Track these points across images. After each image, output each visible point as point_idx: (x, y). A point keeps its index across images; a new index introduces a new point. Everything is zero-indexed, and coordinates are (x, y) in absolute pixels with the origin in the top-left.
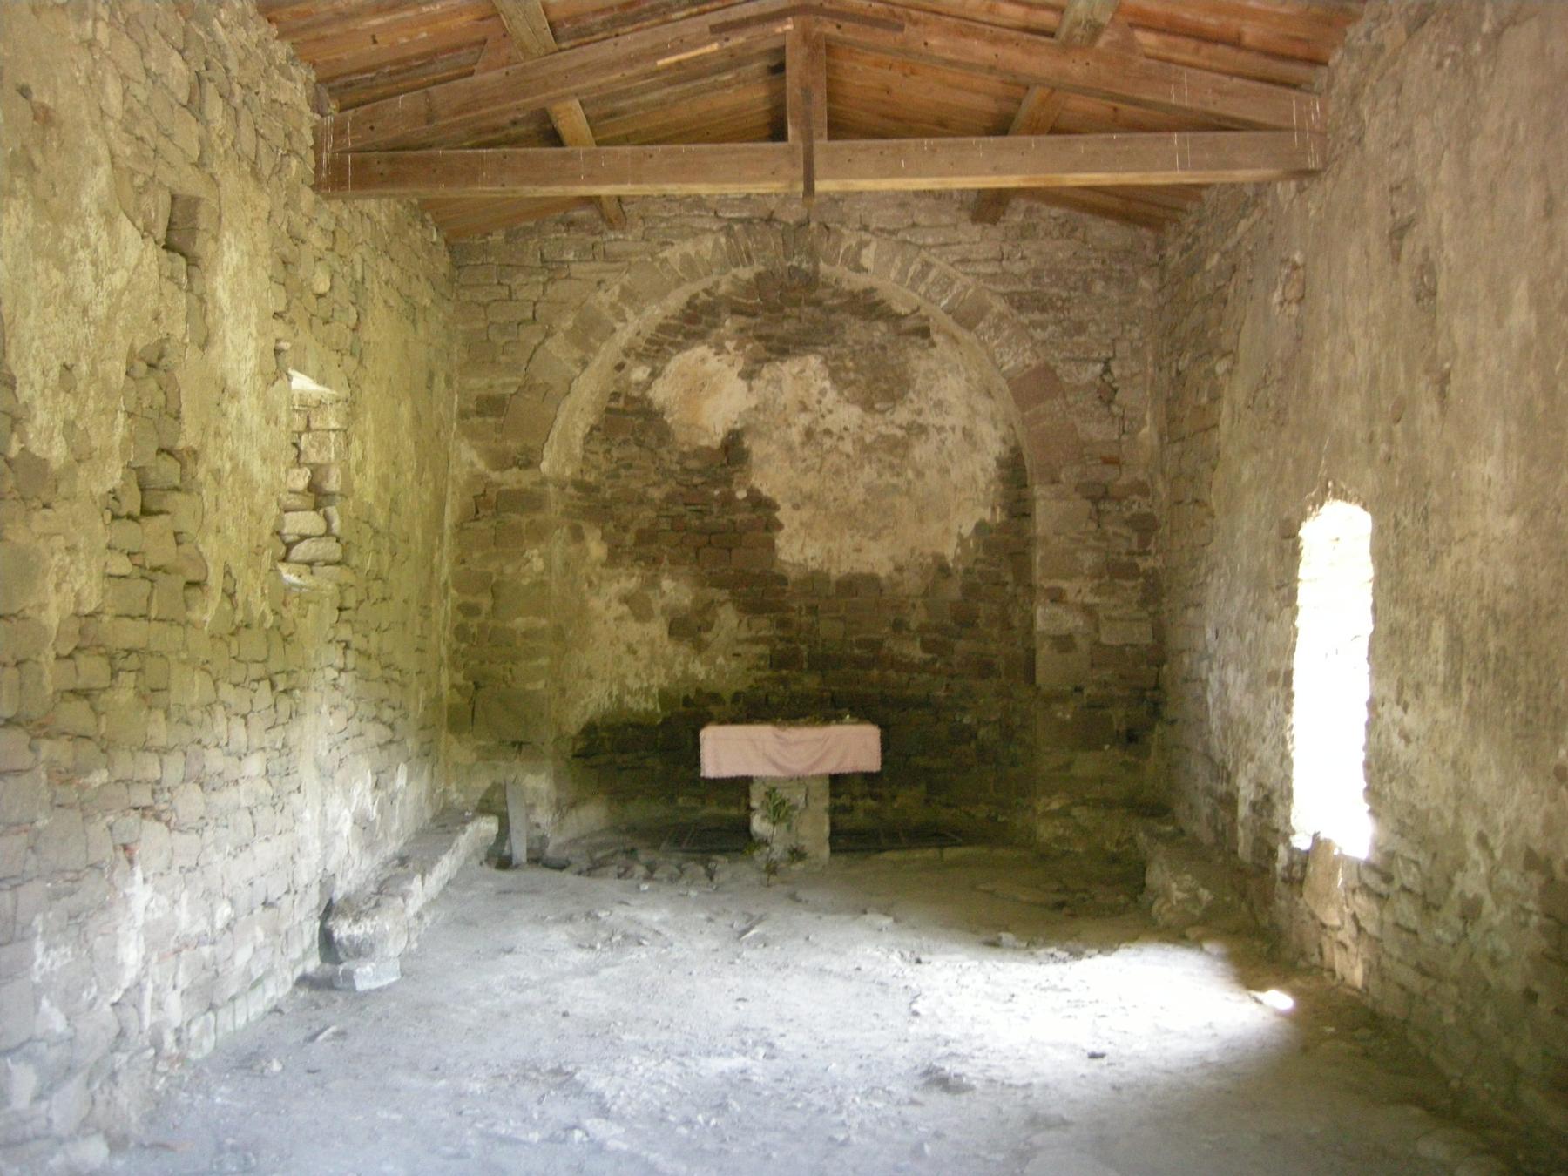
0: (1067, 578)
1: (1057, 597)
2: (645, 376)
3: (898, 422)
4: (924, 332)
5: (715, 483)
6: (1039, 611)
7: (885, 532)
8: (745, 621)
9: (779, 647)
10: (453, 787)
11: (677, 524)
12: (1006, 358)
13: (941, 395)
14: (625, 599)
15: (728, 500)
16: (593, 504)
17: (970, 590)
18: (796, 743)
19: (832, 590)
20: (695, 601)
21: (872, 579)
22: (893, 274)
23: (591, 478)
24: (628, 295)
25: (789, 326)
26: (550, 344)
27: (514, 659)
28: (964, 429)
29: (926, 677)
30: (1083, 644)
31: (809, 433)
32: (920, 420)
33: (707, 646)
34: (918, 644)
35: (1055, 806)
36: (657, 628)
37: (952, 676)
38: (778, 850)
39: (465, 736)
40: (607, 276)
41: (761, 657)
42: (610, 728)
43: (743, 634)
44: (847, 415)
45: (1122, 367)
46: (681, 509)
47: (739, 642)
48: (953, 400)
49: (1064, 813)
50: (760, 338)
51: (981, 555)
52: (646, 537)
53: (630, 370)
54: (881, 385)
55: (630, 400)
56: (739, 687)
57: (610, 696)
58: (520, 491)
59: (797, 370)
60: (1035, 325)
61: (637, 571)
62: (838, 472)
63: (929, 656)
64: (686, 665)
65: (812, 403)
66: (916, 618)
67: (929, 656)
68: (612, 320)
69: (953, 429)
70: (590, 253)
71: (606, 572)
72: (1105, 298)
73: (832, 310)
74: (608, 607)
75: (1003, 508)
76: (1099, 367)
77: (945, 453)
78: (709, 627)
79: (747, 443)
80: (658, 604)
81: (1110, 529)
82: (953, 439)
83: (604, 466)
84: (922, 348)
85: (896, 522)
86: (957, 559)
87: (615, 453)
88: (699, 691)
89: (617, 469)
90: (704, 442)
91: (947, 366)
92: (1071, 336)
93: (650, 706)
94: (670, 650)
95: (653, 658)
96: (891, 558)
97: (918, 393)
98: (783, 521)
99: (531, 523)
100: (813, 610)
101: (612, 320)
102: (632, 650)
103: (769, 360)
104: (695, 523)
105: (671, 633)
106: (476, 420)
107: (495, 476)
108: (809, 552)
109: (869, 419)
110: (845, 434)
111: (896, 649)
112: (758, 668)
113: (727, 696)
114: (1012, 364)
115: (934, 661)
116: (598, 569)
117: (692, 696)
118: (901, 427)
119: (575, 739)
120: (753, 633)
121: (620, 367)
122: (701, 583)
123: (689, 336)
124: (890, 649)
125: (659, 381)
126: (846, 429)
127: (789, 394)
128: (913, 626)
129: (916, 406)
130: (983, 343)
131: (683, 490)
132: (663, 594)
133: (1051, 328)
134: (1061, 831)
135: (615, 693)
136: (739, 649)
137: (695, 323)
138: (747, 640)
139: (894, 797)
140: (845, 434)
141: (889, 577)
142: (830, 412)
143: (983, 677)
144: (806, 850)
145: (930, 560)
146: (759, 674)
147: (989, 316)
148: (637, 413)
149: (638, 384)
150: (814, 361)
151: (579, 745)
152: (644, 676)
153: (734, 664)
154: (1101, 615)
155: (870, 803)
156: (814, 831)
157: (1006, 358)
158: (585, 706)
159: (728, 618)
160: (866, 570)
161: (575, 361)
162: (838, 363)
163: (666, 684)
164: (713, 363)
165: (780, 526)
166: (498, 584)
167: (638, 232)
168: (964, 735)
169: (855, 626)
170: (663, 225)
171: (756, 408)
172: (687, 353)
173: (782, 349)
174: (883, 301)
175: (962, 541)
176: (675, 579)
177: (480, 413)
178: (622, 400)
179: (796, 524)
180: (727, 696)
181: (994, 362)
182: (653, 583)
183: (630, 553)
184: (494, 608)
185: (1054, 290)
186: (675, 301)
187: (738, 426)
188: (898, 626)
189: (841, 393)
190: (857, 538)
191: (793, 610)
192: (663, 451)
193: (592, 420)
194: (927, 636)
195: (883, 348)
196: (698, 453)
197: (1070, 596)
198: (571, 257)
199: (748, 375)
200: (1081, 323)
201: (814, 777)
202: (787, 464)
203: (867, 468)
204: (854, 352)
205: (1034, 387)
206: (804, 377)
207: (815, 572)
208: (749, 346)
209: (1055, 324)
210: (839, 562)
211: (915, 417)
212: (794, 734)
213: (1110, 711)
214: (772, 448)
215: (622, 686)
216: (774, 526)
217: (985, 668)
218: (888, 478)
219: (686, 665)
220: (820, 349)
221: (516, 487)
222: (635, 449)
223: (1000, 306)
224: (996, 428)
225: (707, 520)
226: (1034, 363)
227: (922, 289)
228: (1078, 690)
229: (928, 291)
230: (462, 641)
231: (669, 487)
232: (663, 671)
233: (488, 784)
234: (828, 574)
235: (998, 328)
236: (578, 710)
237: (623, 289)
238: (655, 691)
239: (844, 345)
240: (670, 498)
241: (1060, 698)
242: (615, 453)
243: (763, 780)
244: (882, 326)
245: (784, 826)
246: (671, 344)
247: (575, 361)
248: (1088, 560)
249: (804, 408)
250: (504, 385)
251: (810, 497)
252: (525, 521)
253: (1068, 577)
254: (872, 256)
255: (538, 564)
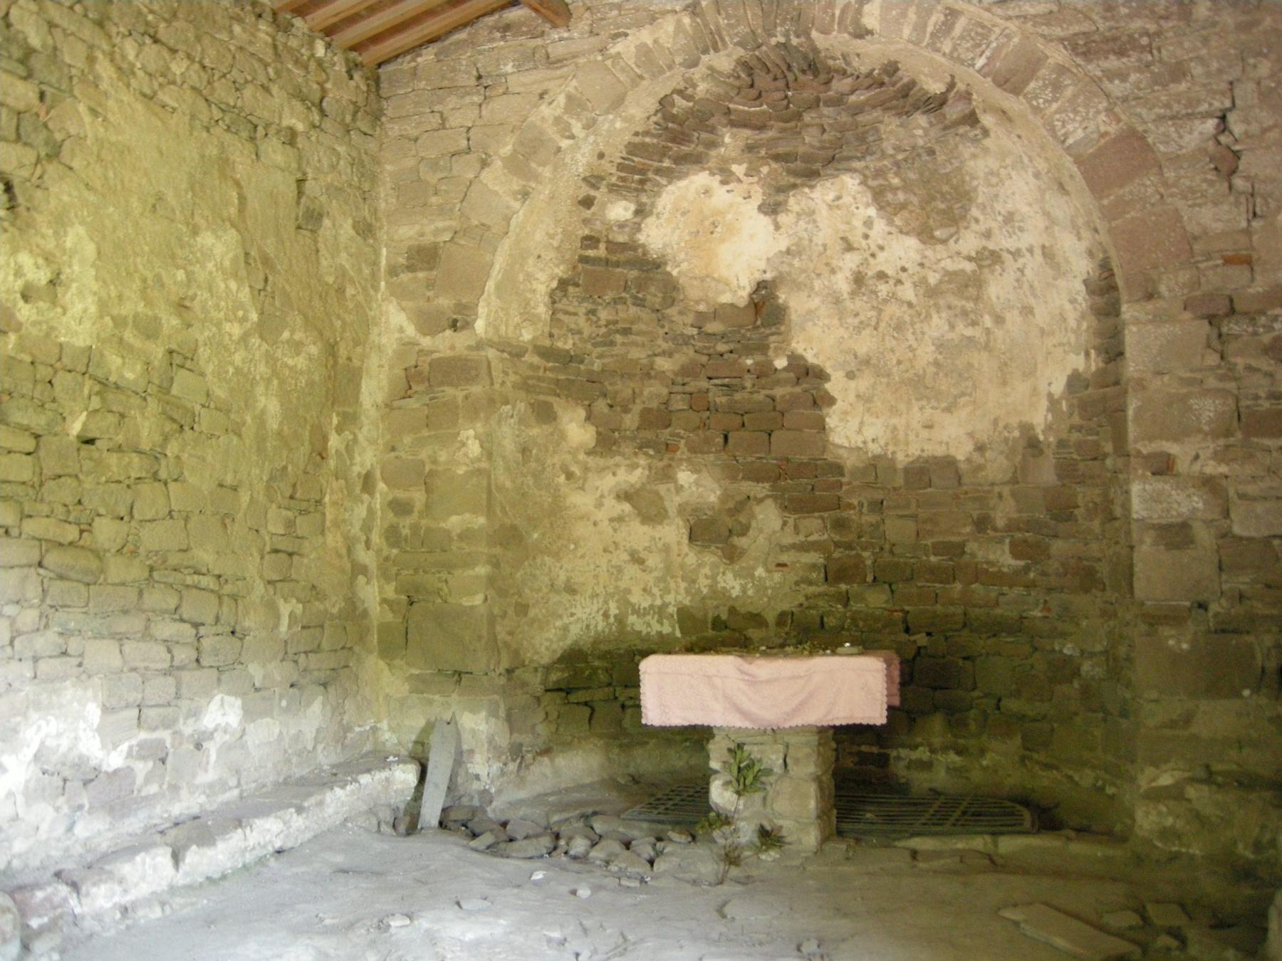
0: (1176, 439)
1: (1163, 467)
2: (628, 215)
3: (965, 253)
4: (971, 119)
5: (749, 351)
6: (1136, 488)
7: (963, 400)
8: (791, 522)
9: (836, 555)
10: (384, 725)
11: (698, 402)
12: (1070, 127)
13: (1009, 207)
14: (625, 496)
15: (764, 373)
16: (561, 376)
17: (1067, 471)
18: (768, 681)
19: (899, 481)
20: (724, 498)
21: (948, 463)
22: (906, 32)
23: (567, 344)
24: (574, 104)
25: (811, 139)
26: (486, 176)
27: (449, 567)
28: (1043, 247)
29: (1019, 590)
30: (1204, 536)
31: (859, 279)
32: (991, 246)
33: (742, 553)
34: (1007, 548)
35: (1166, 780)
36: (673, 532)
37: (1050, 590)
38: (746, 832)
39: (397, 662)
40: (550, 85)
41: (813, 567)
42: (606, 655)
43: (789, 539)
44: (902, 251)
45: (1246, 121)
46: (704, 384)
47: (783, 549)
48: (1025, 209)
49: (1174, 794)
50: (777, 158)
51: (1076, 420)
52: (658, 418)
53: (603, 206)
54: (937, 204)
55: (613, 246)
56: (786, 606)
57: (606, 615)
58: (453, 358)
59: (831, 196)
60: (1111, 75)
61: (642, 461)
62: (899, 327)
63: (1021, 563)
64: (713, 578)
65: (856, 239)
66: (1003, 513)
67: (1021, 563)
68: (557, 137)
69: (1031, 250)
70: (528, 60)
71: (592, 461)
72: (1214, 24)
73: (858, 110)
74: (599, 505)
75: (1099, 353)
76: (1211, 125)
77: (1026, 286)
78: (744, 531)
79: (782, 297)
80: (673, 502)
81: (1240, 362)
82: (1033, 264)
83: (587, 330)
84: (975, 140)
85: (975, 387)
86: (1049, 428)
87: (604, 315)
88: (732, 611)
89: (609, 334)
90: (726, 298)
91: (1008, 161)
92: (1165, 85)
93: (666, 629)
94: (691, 559)
95: (668, 568)
96: (971, 435)
97: (983, 207)
98: (835, 394)
99: (466, 397)
100: (877, 506)
101: (557, 137)
102: (636, 559)
103: (794, 186)
104: (722, 400)
105: (691, 538)
106: (405, 277)
107: (426, 342)
108: (869, 433)
109: (929, 253)
110: (903, 276)
111: (980, 554)
112: (810, 583)
113: (771, 617)
114: (1080, 134)
115: (1027, 569)
116: (582, 457)
117: (724, 617)
118: (970, 259)
119: (548, 669)
120: (801, 538)
121: (587, 202)
122: (732, 473)
123: (680, 159)
124: (973, 555)
125: (651, 220)
126: (904, 269)
127: (826, 230)
128: (1000, 523)
129: (982, 227)
130: (1037, 110)
131: (704, 359)
132: (679, 489)
133: (1133, 77)
134: (1170, 821)
135: (614, 611)
136: (784, 558)
137: (678, 138)
138: (793, 547)
139: (982, 752)
140: (903, 276)
141: (968, 460)
142: (881, 248)
143: (1087, 591)
144: (784, 833)
145: (1016, 434)
146: (812, 589)
147: (1043, 72)
148: (631, 263)
149: (622, 226)
150: (850, 182)
151: (554, 676)
152: (655, 591)
153: (777, 576)
154: (1232, 492)
155: (953, 757)
156: (797, 804)
157: (1070, 127)
158: (565, 629)
159: (768, 518)
160: (940, 451)
161: (515, 193)
162: (881, 181)
163: (687, 602)
164: (722, 196)
165: (831, 401)
166: (432, 474)
167: (584, 25)
168: (1065, 670)
169: (928, 527)
170: (615, 13)
171: (788, 252)
172: (682, 183)
173: (809, 170)
174: (913, 83)
175: (1053, 402)
176: (696, 471)
177: (410, 268)
178: (602, 246)
179: (852, 398)
180: (771, 617)
181: (1053, 130)
182: (666, 475)
183: (633, 439)
184: (428, 506)
185: (1137, 24)
186: (640, 108)
187: (768, 276)
188: (982, 524)
189: (890, 222)
190: (928, 411)
191: (850, 506)
192: (672, 311)
193: (560, 271)
194: (1018, 535)
195: (931, 152)
196: (717, 313)
197: (1182, 466)
198: (509, 68)
199: (772, 209)
200: (1180, 63)
201: (797, 730)
202: (836, 322)
203: (935, 316)
204: (897, 164)
205: (1113, 166)
206: (840, 204)
207: (876, 457)
208: (765, 170)
209: (1139, 70)
210: (907, 444)
211: (985, 243)
212: (764, 667)
213: (1249, 639)
214: (816, 302)
215: (624, 602)
216: (822, 401)
217: (1087, 578)
218: (964, 330)
219: (713, 578)
220: (857, 164)
221: (449, 353)
222: (633, 310)
223: (1058, 55)
224: (1079, 239)
225: (738, 396)
226: (1113, 129)
227: (947, 46)
228: (1202, 606)
229: (955, 49)
230: (392, 545)
231: (685, 356)
232: (683, 585)
233: (422, 722)
234: (893, 460)
235: (1057, 87)
236: (551, 634)
237: (570, 98)
238: (672, 609)
239: (884, 156)
240: (688, 371)
241: (1173, 618)
242: (604, 315)
243: (727, 732)
244: (921, 120)
245: (758, 796)
246: (658, 171)
247: (515, 193)
248: (1208, 409)
249: (849, 248)
250: (437, 232)
251: (867, 362)
252: (460, 395)
253: (1178, 436)
254: (877, 12)
255: (474, 448)
